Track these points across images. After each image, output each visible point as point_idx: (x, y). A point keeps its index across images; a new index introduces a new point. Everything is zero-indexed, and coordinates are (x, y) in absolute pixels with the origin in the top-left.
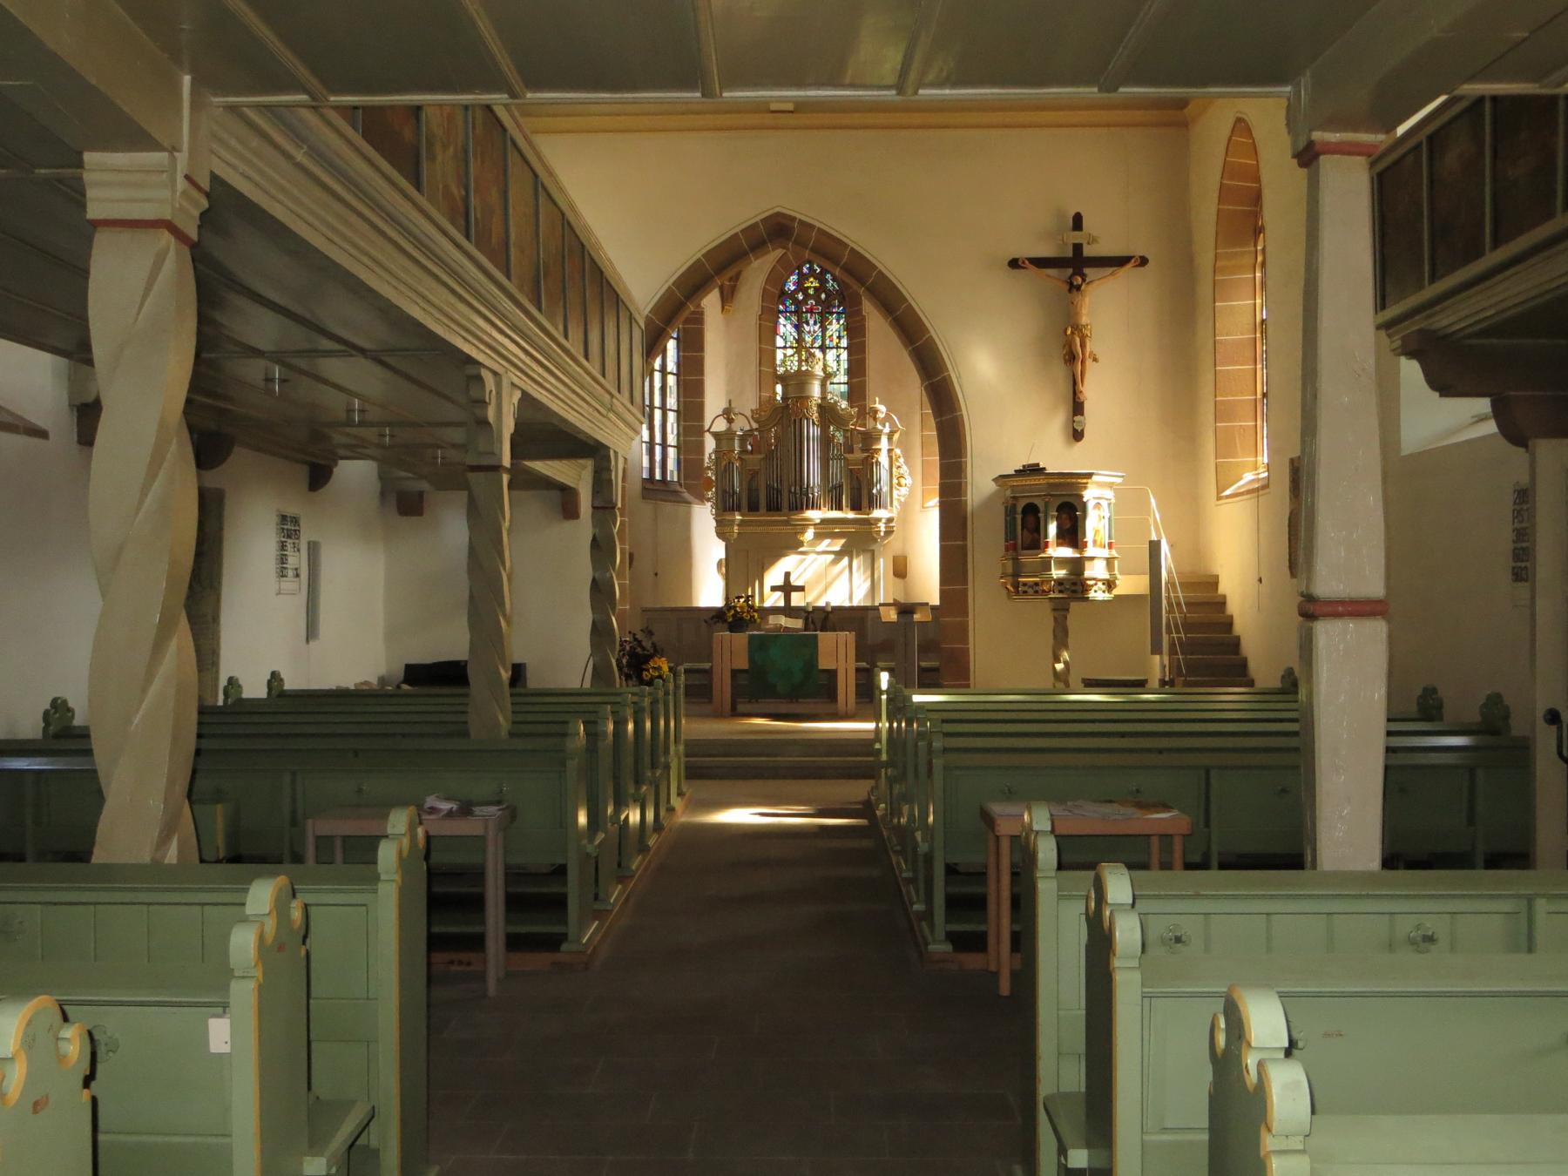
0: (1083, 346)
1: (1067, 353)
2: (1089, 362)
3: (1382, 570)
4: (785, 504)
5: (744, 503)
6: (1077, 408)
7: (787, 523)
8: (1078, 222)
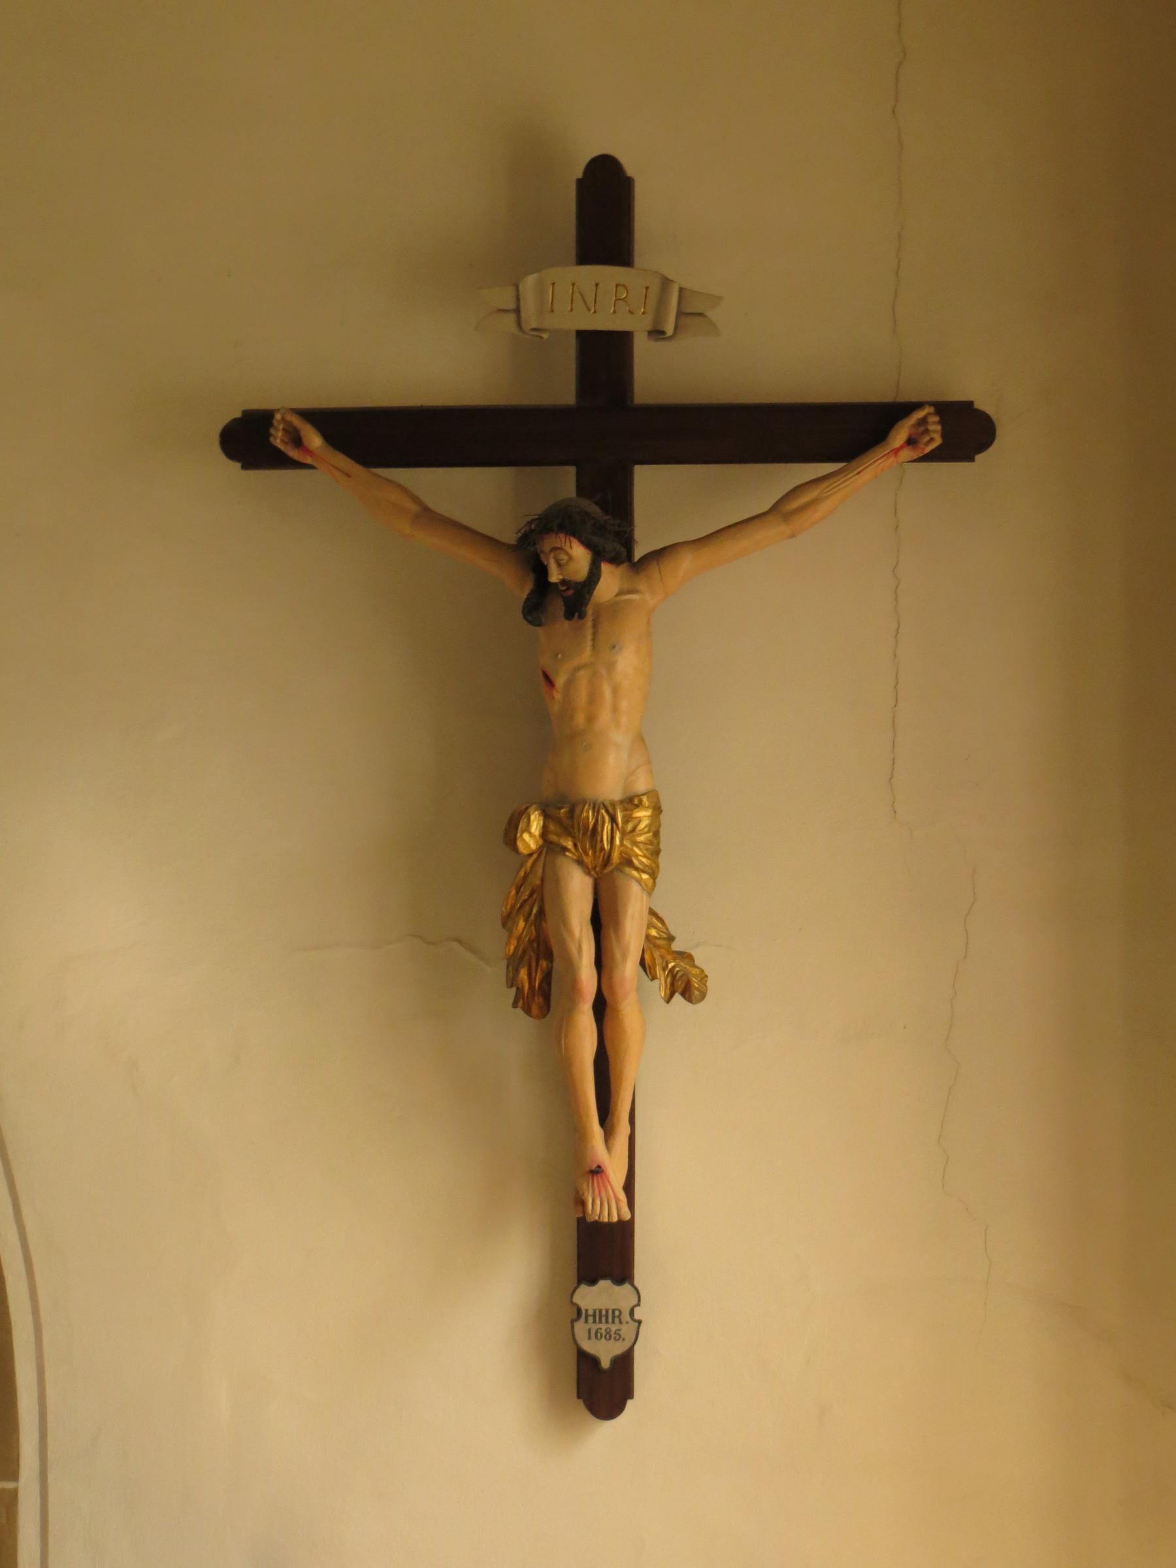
0: (602, 920)
1: (524, 930)
2: (644, 1010)
3: (575, 1375)
6: (603, 1252)
8: (604, 214)
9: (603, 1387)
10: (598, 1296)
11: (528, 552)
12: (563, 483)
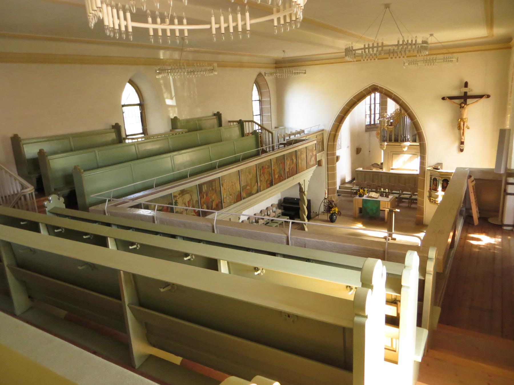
0: (464, 125)
1: (459, 125)
2: (466, 129)
4: (399, 140)
5: (388, 139)
6: (462, 143)
7: (400, 145)
8: (466, 85)
9: (462, 150)
10: (462, 145)
11: (460, 105)
12: (462, 100)
